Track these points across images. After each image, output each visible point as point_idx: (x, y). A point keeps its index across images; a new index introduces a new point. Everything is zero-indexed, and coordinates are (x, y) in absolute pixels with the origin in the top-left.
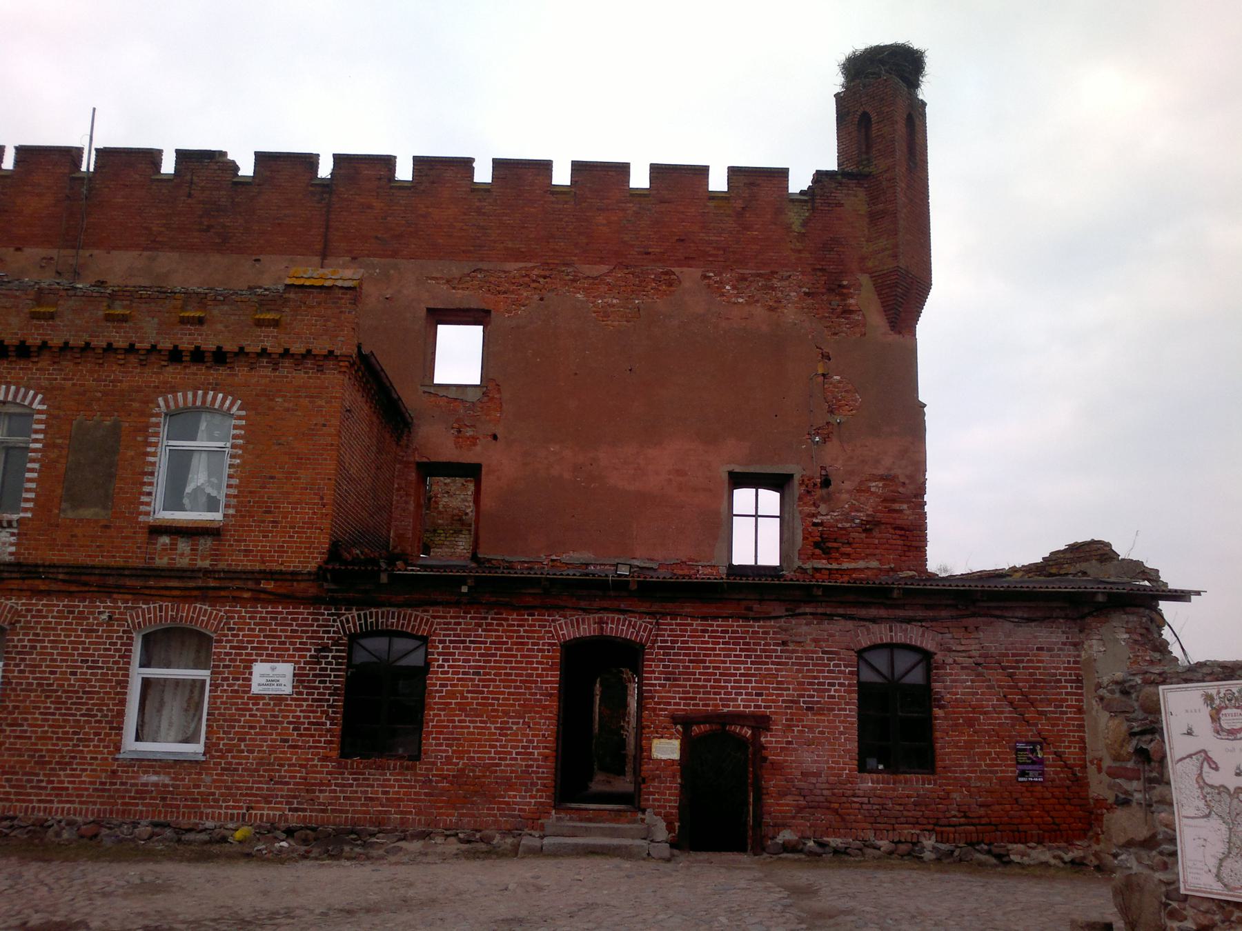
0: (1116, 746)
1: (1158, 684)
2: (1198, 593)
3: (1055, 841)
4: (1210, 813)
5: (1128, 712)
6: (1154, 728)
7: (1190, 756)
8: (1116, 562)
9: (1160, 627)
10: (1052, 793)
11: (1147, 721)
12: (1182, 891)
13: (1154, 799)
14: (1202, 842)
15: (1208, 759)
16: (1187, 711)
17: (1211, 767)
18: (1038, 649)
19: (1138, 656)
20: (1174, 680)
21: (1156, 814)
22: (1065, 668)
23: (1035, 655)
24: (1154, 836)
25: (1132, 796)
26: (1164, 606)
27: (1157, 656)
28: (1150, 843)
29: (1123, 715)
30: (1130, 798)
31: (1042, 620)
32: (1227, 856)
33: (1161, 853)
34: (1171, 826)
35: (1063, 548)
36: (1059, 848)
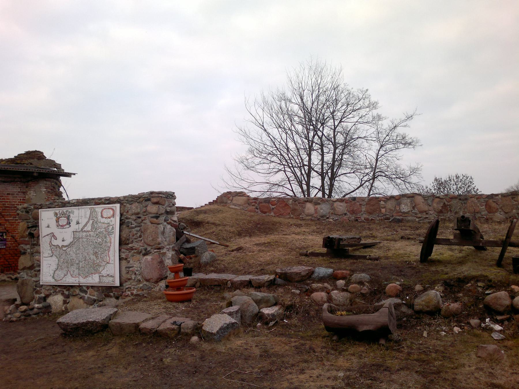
0: (22, 232)
1: (39, 209)
2: (74, 174)
3: (9, 271)
4: (53, 255)
5: (28, 219)
6: (36, 225)
7: (48, 235)
8: (44, 160)
9: (59, 187)
10: (9, 252)
11: (34, 223)
12: (41, 284)
13: (34, 251)
14: (49, 265)
15: (54, 236)
16: (48, 219)
17: (54, 239)
18: (7, 194)
19: (49, 198)
20: (45, 207)
21: (34, 257)
22: (19, 202)
23: (6, 197)
24: (33, 265)
25: (27, 251)
26: (62, 178)
27: (57, 197)
28: (31, 268)
29: (26, 221)
30: (26, 251)
31: (11, 182)
32: (57, 269)
33: (35, 271)
34: (39, 261)
35: (23, 153)
36: (10, 274)
